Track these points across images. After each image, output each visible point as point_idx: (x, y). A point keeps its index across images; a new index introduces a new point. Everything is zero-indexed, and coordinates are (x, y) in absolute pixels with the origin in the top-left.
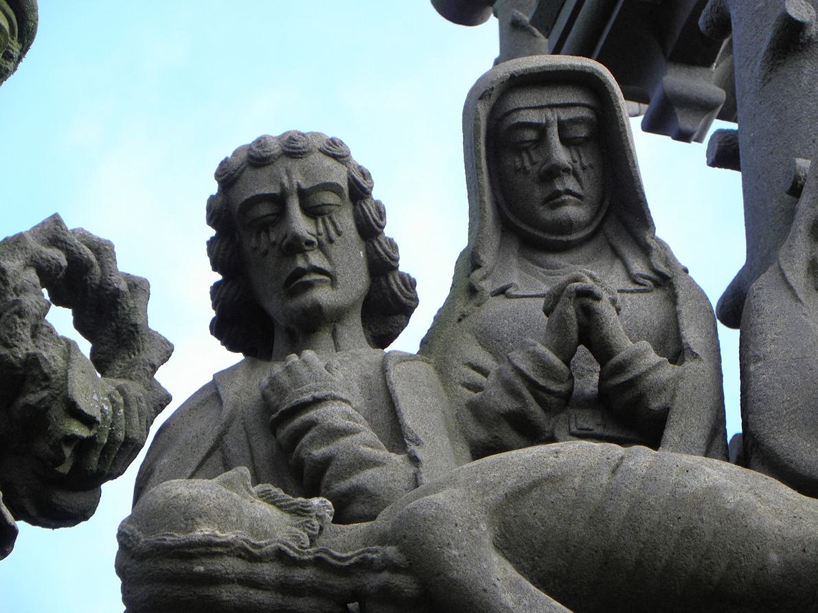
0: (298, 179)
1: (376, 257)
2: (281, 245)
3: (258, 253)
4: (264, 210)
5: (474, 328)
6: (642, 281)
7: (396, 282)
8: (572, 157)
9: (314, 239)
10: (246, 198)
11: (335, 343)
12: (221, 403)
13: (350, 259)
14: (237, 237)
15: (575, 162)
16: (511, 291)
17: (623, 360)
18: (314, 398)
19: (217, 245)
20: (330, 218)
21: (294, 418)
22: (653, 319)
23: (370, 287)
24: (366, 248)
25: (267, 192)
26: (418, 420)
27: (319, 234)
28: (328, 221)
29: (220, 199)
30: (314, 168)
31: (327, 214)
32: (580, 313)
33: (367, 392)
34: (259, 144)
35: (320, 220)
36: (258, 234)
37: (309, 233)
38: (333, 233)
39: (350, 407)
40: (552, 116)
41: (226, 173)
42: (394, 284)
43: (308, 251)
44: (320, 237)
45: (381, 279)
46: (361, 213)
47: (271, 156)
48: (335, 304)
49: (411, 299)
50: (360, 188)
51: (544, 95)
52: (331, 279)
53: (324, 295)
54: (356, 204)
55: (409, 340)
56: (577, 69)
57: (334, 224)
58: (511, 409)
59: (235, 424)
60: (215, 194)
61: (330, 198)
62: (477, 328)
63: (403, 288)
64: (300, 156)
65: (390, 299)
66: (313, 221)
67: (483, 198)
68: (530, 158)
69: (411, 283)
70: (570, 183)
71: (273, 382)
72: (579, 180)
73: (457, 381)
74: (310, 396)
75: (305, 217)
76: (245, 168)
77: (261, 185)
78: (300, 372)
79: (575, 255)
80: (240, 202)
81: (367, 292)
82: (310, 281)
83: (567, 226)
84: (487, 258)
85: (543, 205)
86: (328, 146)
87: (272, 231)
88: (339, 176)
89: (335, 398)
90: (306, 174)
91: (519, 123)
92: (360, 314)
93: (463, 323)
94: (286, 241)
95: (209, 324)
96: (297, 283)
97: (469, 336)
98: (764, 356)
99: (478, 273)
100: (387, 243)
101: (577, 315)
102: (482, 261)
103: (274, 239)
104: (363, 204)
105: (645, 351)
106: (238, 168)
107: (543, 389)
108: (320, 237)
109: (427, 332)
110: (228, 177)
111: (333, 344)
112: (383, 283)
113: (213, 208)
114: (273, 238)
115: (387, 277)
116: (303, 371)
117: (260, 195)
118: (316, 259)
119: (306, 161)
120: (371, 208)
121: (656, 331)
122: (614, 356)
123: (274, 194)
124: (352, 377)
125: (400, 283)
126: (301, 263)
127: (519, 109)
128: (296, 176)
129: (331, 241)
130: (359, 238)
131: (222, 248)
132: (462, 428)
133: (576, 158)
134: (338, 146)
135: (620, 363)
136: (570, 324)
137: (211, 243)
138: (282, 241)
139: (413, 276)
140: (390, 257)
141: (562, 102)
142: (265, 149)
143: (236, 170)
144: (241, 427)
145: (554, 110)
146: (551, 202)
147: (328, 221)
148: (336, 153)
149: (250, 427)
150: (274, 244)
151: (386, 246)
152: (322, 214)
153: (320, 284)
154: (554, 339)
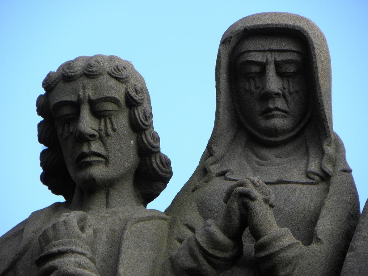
0: (90, 93)
4: (66, 111)
5: (198, 199)
6: (312, 176)
8: (283, 85)
9: (96, 133)
11: (107, 201)
15: (284, 88)
16: (228, 175)
17: (264, 242)
20: (110, 119)
22: (311, 205)
23: (140, 163)
24: (137, 138)
26: (130, 268)
27: (100, 130)
30: (101, 86)
31: (108, 116)
32: (241, 207)
35: (103, 120)
37: (93, 129)
38: (110, 129)
40: (271, 57)
42: (155, 163)
43: (91, 140)
44: (100, 132)
45: (147, 159)
48: (106, 177)
49: (166, 172)
51: (267, 42)
52: (106, 160)
55: (161, 203)
56: (290, 27)
58: (190, 266)
61: (110, 106)
62: (200, 199)
63: (161, 165)
64: (93, 77)
66: (98, 121)
67: (219, 110)
68: (255, 84)
70: (280, 103)
72: (287, 101)
73: (175, 237)
74: (57, 249)
75: (93, 118)
76: (60, 81)
79: (276, 151)
82: (90, 161)
83: (275, 132)
84: (218, 151)
85: (261, 115)
86: (113, 71)
88: (118, 91)
89: (73, 252)
90: (95, 89)
91: (248, 60)
93: (195, 193)
97: (194, 204)
98: (355, 248)
99: (210, 160)
100: (150, 136)
101: (240, 209)
102: (214, 152)
105: (281, 236)
106: (55, 81)
107: (212, 256)
108: (100, 132)
109: (176, 194)
112: (148, 161)
117: (65, 101)
118: (96, 147)
120: (140, 113)
121: (311, 214)
122: (261, 238)
123: (73, 102)
125: (158, 162)
126: (85, 149)
127: (249, 51)
128: (89, 91)
129: (108, 135)
130: (131, 132)
131: (44, 131)
132: (163, 274)
133: (286, 86)
135: (262, 244)
136: (233, 214)
137: (40, 125)
140: (151, 146)
141: (278, 48)
142: (71, 71)
143: (53, 82)
145: (273, 53)
146: (266, 115)
147: (108, 121)
150: (72, 133)
152: (104, 117)
153: (96, 163)
154: (223, 223)
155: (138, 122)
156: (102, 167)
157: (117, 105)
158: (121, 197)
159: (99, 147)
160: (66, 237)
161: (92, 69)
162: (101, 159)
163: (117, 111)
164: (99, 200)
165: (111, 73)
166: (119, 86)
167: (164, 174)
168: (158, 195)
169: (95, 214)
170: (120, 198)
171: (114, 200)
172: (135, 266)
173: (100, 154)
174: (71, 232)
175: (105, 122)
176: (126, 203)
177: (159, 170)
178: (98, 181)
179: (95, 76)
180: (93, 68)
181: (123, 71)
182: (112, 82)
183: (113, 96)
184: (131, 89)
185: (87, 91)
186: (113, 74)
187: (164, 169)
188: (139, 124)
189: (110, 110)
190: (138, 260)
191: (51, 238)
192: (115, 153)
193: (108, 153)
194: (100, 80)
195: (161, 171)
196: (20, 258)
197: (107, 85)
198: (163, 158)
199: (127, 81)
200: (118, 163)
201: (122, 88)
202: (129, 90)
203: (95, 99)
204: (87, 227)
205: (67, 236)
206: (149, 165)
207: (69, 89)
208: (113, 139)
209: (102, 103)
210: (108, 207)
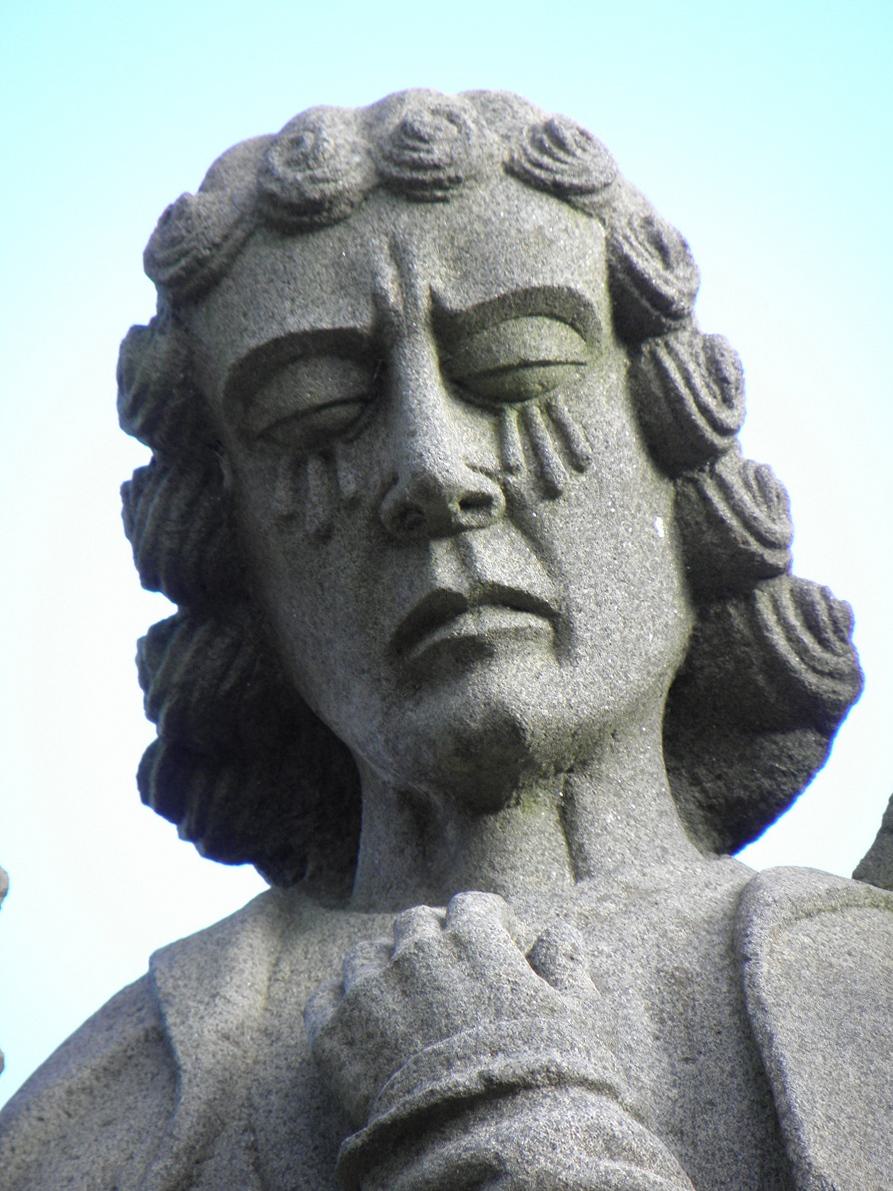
0: (433, 276)
1: (709, 537)
2: (376, 508)
3: (300, 535)
4: (319, 385)
7: (782, 621)
9: (492, 488)
10: (253, 343)
11: (569, 844)
12: (174, 1074)
13: (618, 552)
14: (225, 472)
18: (487, 1079)
19: (156, 500)
21: (420, 1151)
23: (694, 638)
25: (326, 325)
28: (540, 419)
29: (163, 344)
33: (680, 1033)
34: (296, 153)
35: (512, 417)
36: (298, 467)
37: (474, 468)
39: (614, 1106)
41: (185, 253)
43: (471, 528)
44: (512, 479)
45: (732, 611)
46: (656, 388)
47: (339, 196)
50: (649, 300)
53: (526, 684)
54: (639, 352)
57: (560, 429)
59: (221, 1146)
60: (145, 321)
61: (546, 339)
63: (808, 639)
64: (439, 194)
65: (761, 679)
66: (484, 425)
69: (835, 622)
71: (352, 1013)
77: (309, 298)
78: (444, 981)
80: (231, 359)
81: (681, 657)
86: (535, 154)
87: (347, 457)
89: (560, 1080)
90: (463, 257)
92: (657, 736)
94: (394, 495)
95: (135, 770)
96: (431, 643)
103: (352, 487)
104: (662, 353)
106: (226, 238)
108: (512, 479)
110: (189, 271)
111: (563, 851)
113: (138, 376)
114: (349, 485)
115: (750, 600)
116: (451, 974)
118: (499, 556)
119: (461, 209)
120: (691, 367)
124: (627, 979)
126: (446, 573)
129: (550, 491)
130: (650, 474)
131: (174, 515)
134: (568, 152)
137: (135, 491)
138: (383, 496)
139: (838, 594)
142: (318, 173)
143: (217, 246)
144: (243, 1160)
147: (540, 419)
148: (566, 179)
149: (275, 1164)
150: (354, 503)
151: (747, 498)
152: (520, 396)
155: (690, 415)
156: (539, 663)
157: (577, 330)
158: (636, 820)
159: (516, 556)
160: (446, 1026)
161: (429, 152)
162: (533, 623)
163: (582, 364)
164: (534, 840)
165: (528, 166)
166: (577, 232)
167: (827, 685)
168: (783, 803)
169: (544, 906)
170: (632, 822)
171: (609, 833)
172: (869, 1130)
173: (528, 596)
174: (508, 987)
175: (526, 423)
176: (664, 850)
177: (803, 666)
178: (533, 735)
179: (446, 189)
180: (435, 147)
181: (584, 150)
182: (538, 212)
183: (559, 280)
184: (635, 243)
185: (417, 267)
186: (537, 172)
187: (827, 656)
188: (695, 427)
189: (551, 358)
190: (871, 1101)
191: (401, 1028)
192: (596, 584)
193: (566, 588)
194: (475, 209)
195: (815, 670)
196: (195, 1173)
197: (519, 231)
198: (817, 597)
199: (607, 203)
200: (617, 636)
201: (589, 241)
202: (626, 248)
203: (470, 304)
204: (562, 960)
205: (492, 1010)
206: (748, 645)
207: (318, 267)
208: (579, 511)
209: (502, 326)
210: (589, 873)
